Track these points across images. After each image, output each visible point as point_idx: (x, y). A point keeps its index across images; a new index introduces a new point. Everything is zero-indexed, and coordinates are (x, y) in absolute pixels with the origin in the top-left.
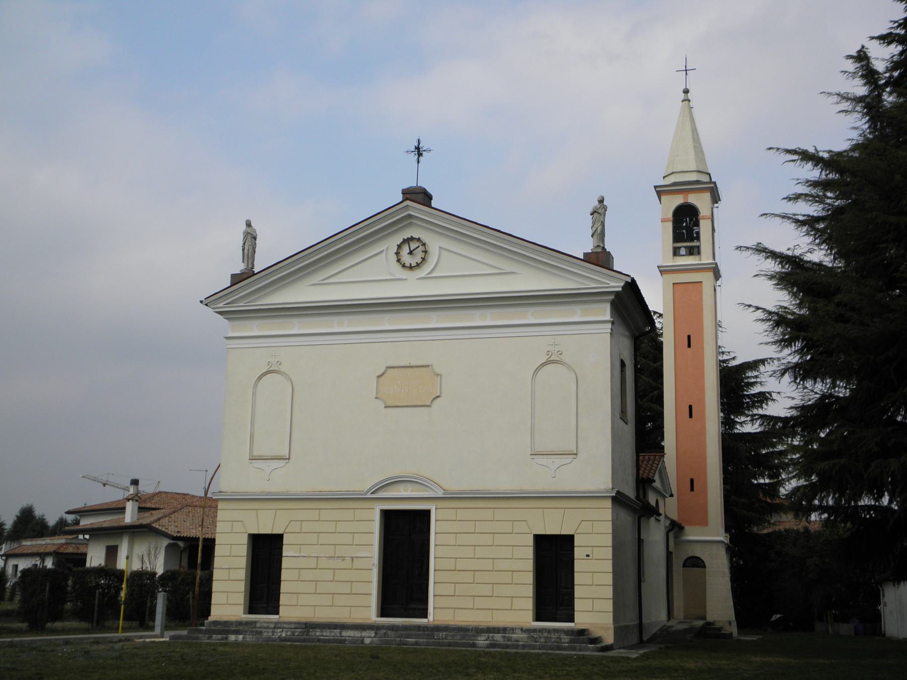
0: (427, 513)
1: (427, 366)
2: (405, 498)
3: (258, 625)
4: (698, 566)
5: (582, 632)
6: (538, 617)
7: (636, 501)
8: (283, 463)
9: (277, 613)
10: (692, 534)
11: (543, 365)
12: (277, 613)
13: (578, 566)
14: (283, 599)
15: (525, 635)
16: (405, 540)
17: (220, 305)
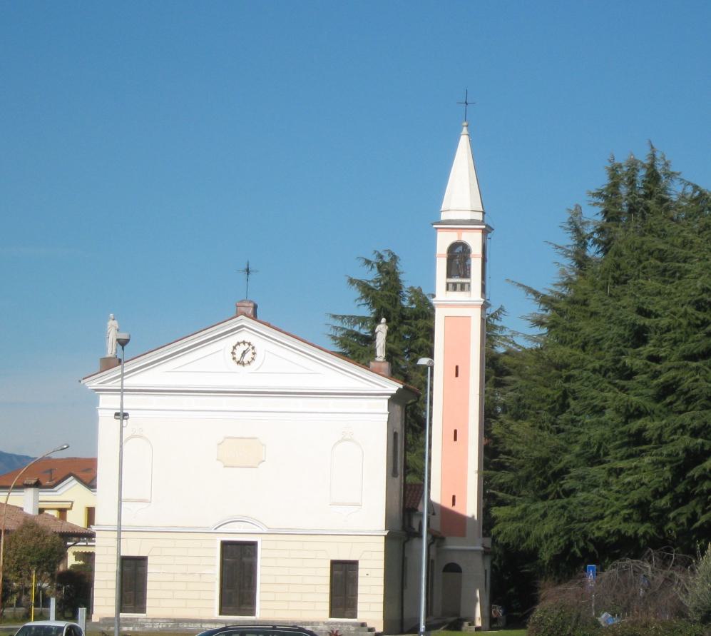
0: (254, 544)
1: (255, 438)
2: (239, 533)
3: (140, 620)
4: (457, 572)
5: (363, 625)
6: (331, 615)
7: (402, 532)
8: (145, 505)
9: (356, 617)
10: (453, 544)
11: (339, 442)
12: (356, 617)
13: (361, 581)
14: (149, 603)
15: (326, 627)
16: (238, 564)
17: (94, 384)
